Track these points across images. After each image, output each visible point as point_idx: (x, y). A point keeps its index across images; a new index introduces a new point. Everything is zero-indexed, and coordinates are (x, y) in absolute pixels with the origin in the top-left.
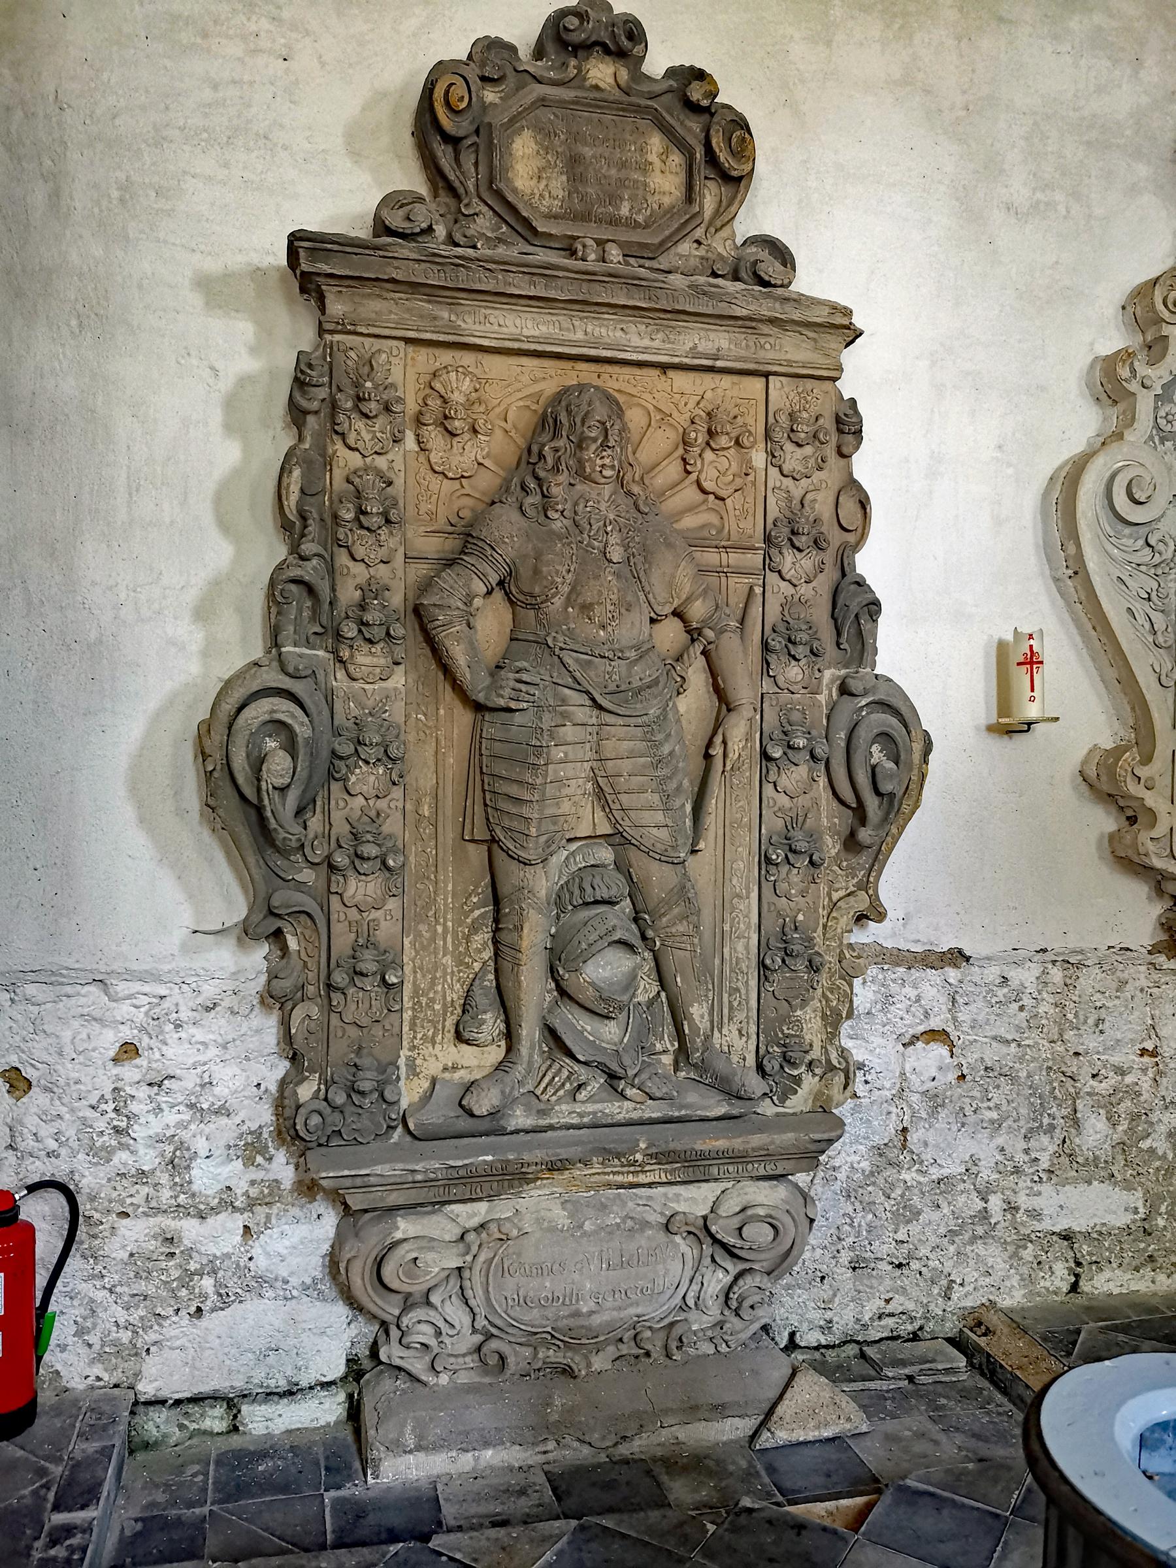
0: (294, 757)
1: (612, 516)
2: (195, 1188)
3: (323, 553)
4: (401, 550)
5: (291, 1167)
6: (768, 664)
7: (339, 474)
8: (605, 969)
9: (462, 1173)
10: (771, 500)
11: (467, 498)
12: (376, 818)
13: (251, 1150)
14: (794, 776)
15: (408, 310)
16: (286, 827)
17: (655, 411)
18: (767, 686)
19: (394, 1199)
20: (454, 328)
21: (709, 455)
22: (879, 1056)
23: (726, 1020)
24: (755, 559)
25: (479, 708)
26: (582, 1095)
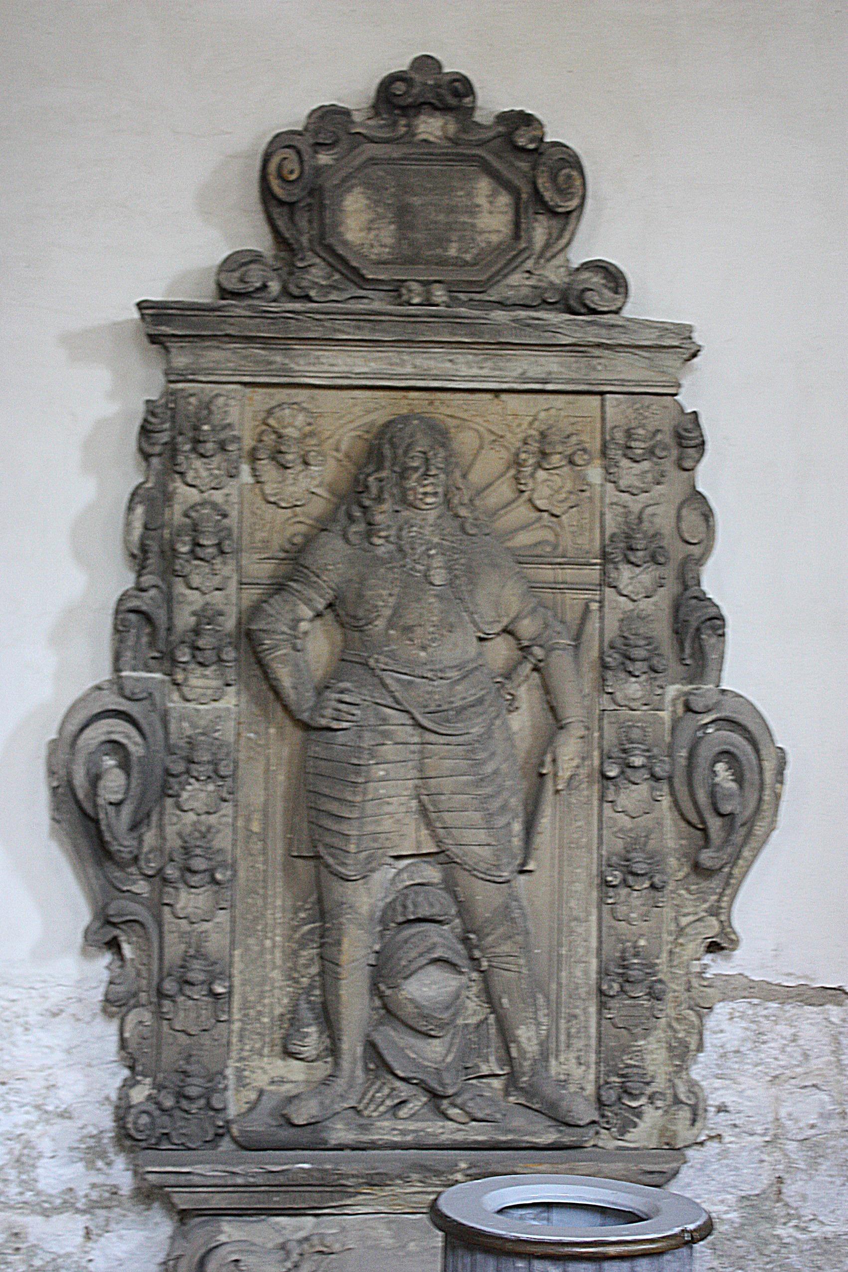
0: (128, 775)
1: (436, 540)
2: (40, 1186)
3: (160, 583)
4: (235, 577)
5: (129, 1174)
6: (604, 680)
7: (178, 509)
8: (426, 987)
9: (281, 1179)
10: (608, 516)
11: (299, 526)
12: (206, 834)
13: (92, 1154)
14: (633, 796)
15: (245, 357)
16: (122, 842)
17: (485, 436)
18: (605, 700)
19: (218, 1201)
20: (284, 370)
21: (541, 474)
22: (749, 1099)
23: (563, 1046)
24: (593, 574)
25: (306, 727)
26: (403, 1112)
